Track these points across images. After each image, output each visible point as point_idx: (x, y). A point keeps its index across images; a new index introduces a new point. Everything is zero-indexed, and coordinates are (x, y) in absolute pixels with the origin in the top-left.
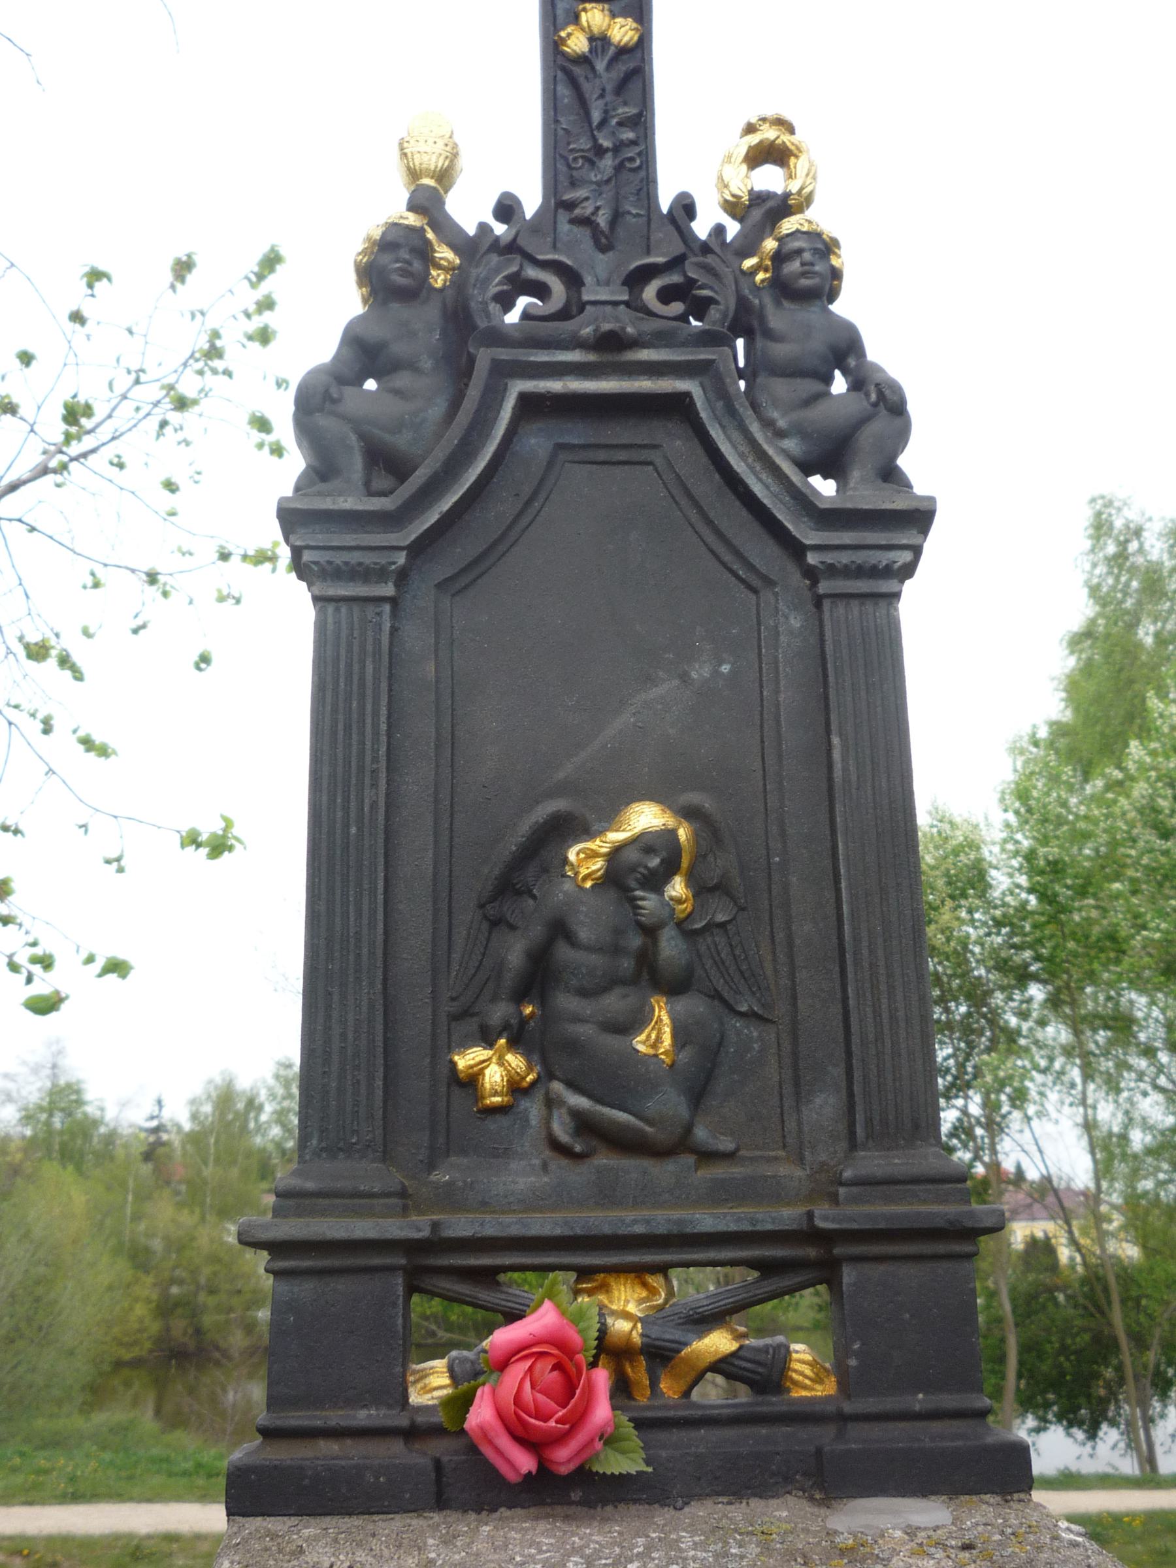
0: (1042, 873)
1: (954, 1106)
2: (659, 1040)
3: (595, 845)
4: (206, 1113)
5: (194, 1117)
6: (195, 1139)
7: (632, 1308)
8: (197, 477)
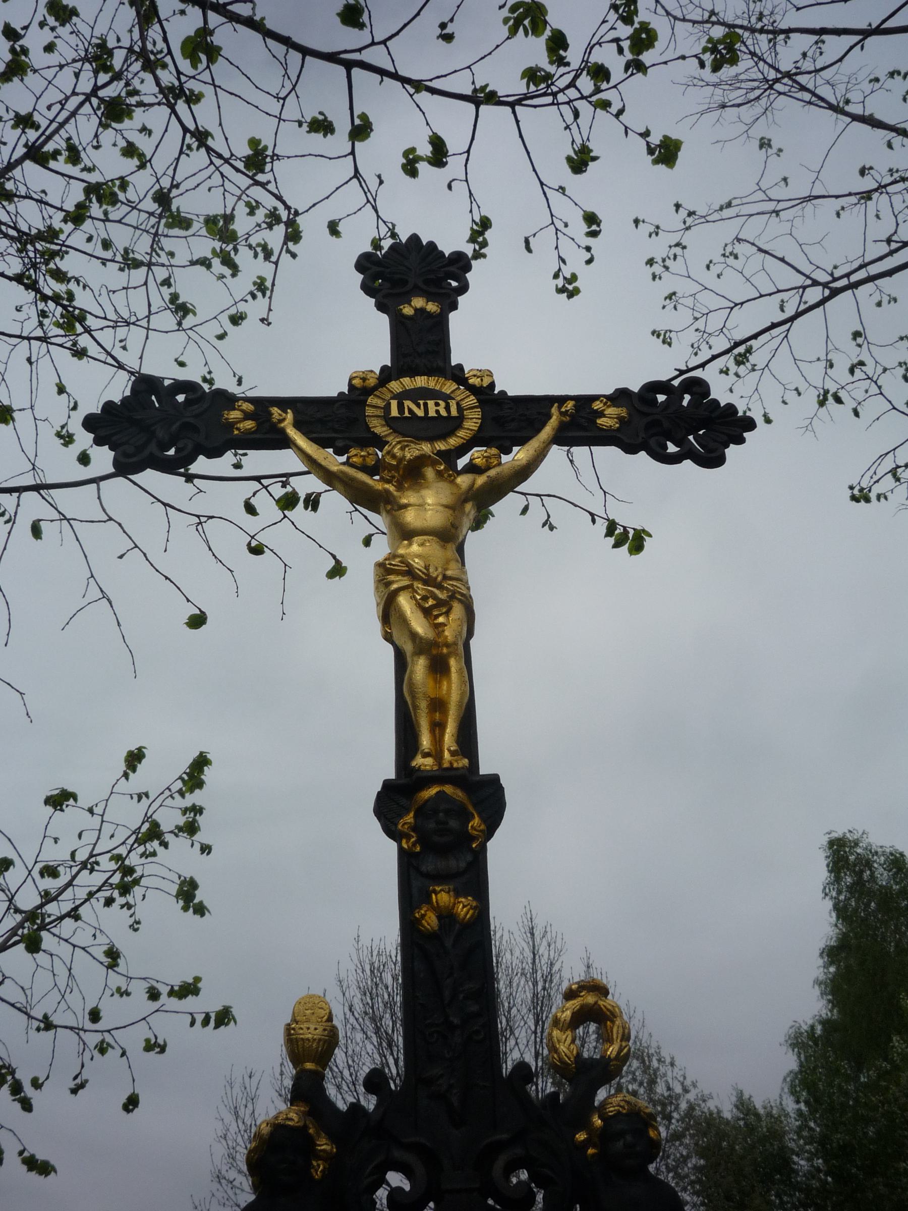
8: (136, 926)
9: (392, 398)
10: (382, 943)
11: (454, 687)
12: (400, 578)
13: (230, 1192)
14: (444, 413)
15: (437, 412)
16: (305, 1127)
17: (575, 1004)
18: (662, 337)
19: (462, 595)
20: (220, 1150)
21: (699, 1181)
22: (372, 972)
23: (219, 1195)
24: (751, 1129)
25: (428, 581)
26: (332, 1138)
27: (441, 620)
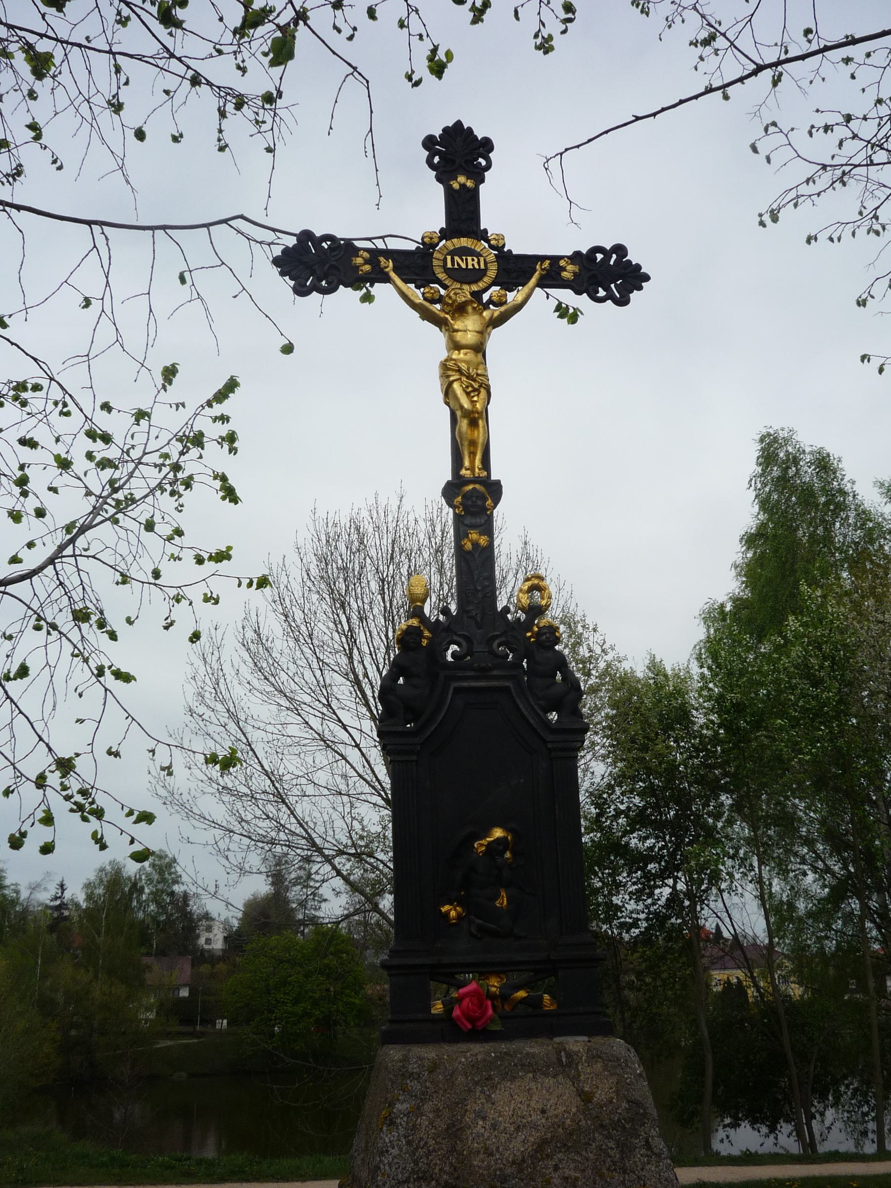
0: (728, 712)
1: (667, 885)
2: (503, 902)
3: (483, 842)
4: (99, 894)
5: (89, 897)
6: (91, 914)
7: (496, 984)
9: (448, 254)
10: (337, 516)
11: (481, 435)
12: (454, 373)
13: (201, 723)
14: (477, 267)
15: (473, 265)
16: (420, 627)
17: (529, 583)
18: (640, 7)
19: (486, 385)
20: (191, 690)
21: (610, 727)
22: (328, 541)
23: (192, 726)
24: (659, 687)
25: (469, 377)
26: (429, 631)
27: (475, 399)
